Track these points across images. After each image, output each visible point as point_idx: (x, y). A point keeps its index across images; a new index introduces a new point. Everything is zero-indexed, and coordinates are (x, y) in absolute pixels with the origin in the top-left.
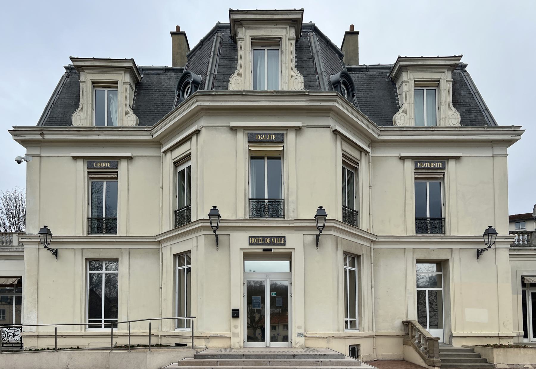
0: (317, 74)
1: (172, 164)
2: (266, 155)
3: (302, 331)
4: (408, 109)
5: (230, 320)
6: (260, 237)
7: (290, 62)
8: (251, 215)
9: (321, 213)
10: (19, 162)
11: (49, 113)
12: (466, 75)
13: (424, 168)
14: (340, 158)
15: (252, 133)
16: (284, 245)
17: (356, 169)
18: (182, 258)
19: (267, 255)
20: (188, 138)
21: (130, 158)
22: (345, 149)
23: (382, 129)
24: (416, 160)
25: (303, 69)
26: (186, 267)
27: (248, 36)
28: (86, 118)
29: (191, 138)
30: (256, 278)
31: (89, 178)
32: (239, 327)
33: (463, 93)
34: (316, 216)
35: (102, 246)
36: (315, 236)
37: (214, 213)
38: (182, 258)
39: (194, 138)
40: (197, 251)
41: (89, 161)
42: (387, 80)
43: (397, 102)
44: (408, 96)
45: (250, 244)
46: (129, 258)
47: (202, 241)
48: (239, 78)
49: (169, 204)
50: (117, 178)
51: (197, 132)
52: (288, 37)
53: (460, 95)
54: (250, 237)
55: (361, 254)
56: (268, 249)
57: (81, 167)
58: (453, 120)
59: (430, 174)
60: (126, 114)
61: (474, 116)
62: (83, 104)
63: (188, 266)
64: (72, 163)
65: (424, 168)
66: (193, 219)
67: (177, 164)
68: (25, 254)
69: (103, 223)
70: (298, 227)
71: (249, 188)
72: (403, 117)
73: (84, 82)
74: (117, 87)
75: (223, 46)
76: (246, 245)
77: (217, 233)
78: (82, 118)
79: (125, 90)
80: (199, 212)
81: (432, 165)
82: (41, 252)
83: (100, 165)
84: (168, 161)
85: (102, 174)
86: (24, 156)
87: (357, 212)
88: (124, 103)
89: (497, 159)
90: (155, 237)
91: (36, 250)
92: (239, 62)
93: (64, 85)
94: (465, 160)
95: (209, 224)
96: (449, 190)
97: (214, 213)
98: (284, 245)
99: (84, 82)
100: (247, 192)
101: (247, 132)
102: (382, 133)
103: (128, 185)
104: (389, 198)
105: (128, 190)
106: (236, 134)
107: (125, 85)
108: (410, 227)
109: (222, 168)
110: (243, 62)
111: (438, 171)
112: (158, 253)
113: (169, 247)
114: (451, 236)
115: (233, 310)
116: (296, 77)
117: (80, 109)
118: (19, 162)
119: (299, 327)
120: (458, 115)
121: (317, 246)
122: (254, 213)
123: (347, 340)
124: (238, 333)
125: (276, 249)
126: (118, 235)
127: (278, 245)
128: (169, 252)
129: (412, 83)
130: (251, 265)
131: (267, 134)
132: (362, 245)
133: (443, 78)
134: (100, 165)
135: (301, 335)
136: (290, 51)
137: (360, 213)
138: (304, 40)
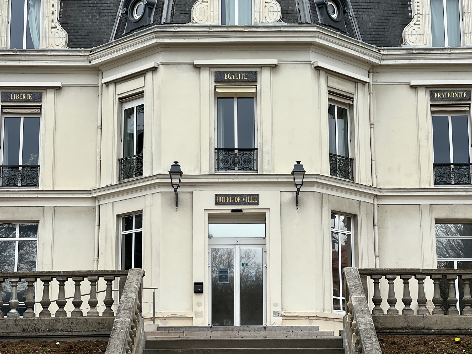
1: (117, 100)
2: (236, 99)
3: (278, 309)
5: (192, 296)
8: (218, 168)
9: (299, 169)
13: (442, 99)
14: (325, 96)
15: (219, 72)
16: (257, 204)
17: (351, 106)
18: (131, 220)
19: (237, 217)
20: (142, 74)
21: (58, 89)
22: (331, 84)
26: (134, 231)
29: (146, 73)
30: (223, 246)
32: (203, 305)
34: (293, 172)
36: (295, 194)
37: (176, 170)
38: (131, 220)
40: (151, 211)
43: (409, 9)
45: (216, 204)
46: (54, 220)
47: (158, 199)
49: (112, 149)
50: (40, 114)
51: (154, 70)
54: (216, 195)
55: (358, 213)
56: (238, 209)
60: (53, 30)
63: (138, 230)
65: (442, 99)
66: (146, 173)
67: (122, 100)
70: (274, 182)
71: (215, 136)
72: (414, 33)
76: (212, 205)
77: (178, 190)
80: (155, 163)
83: (18, 97)
84: (111, 96)
87: (352, 160)
88: (51, 15)
90: (90, 191)
95: (170, 181)
97: (176, 170)
98: (257, 204)
100: (213, 141)
102: (384, 57)
103: (55, 122)
105: (55, 129)
106: (200, 72)
108: (427, 178)
109: (182, 114)
111: (462, 103)
112: (94, 212)
113: (110, 206)
115: (196, 284)
119: (275, 305)
121: (297, 206)
122: (221, 165)
123: (335, 323)
124: (202, 312)
125: (247, 209)
127: (250, 204)
128: (110, 213)
130: (219, 229)
131: (238, 72)
132: (360, 201)
134: (18, 97)
135: (277, 314)
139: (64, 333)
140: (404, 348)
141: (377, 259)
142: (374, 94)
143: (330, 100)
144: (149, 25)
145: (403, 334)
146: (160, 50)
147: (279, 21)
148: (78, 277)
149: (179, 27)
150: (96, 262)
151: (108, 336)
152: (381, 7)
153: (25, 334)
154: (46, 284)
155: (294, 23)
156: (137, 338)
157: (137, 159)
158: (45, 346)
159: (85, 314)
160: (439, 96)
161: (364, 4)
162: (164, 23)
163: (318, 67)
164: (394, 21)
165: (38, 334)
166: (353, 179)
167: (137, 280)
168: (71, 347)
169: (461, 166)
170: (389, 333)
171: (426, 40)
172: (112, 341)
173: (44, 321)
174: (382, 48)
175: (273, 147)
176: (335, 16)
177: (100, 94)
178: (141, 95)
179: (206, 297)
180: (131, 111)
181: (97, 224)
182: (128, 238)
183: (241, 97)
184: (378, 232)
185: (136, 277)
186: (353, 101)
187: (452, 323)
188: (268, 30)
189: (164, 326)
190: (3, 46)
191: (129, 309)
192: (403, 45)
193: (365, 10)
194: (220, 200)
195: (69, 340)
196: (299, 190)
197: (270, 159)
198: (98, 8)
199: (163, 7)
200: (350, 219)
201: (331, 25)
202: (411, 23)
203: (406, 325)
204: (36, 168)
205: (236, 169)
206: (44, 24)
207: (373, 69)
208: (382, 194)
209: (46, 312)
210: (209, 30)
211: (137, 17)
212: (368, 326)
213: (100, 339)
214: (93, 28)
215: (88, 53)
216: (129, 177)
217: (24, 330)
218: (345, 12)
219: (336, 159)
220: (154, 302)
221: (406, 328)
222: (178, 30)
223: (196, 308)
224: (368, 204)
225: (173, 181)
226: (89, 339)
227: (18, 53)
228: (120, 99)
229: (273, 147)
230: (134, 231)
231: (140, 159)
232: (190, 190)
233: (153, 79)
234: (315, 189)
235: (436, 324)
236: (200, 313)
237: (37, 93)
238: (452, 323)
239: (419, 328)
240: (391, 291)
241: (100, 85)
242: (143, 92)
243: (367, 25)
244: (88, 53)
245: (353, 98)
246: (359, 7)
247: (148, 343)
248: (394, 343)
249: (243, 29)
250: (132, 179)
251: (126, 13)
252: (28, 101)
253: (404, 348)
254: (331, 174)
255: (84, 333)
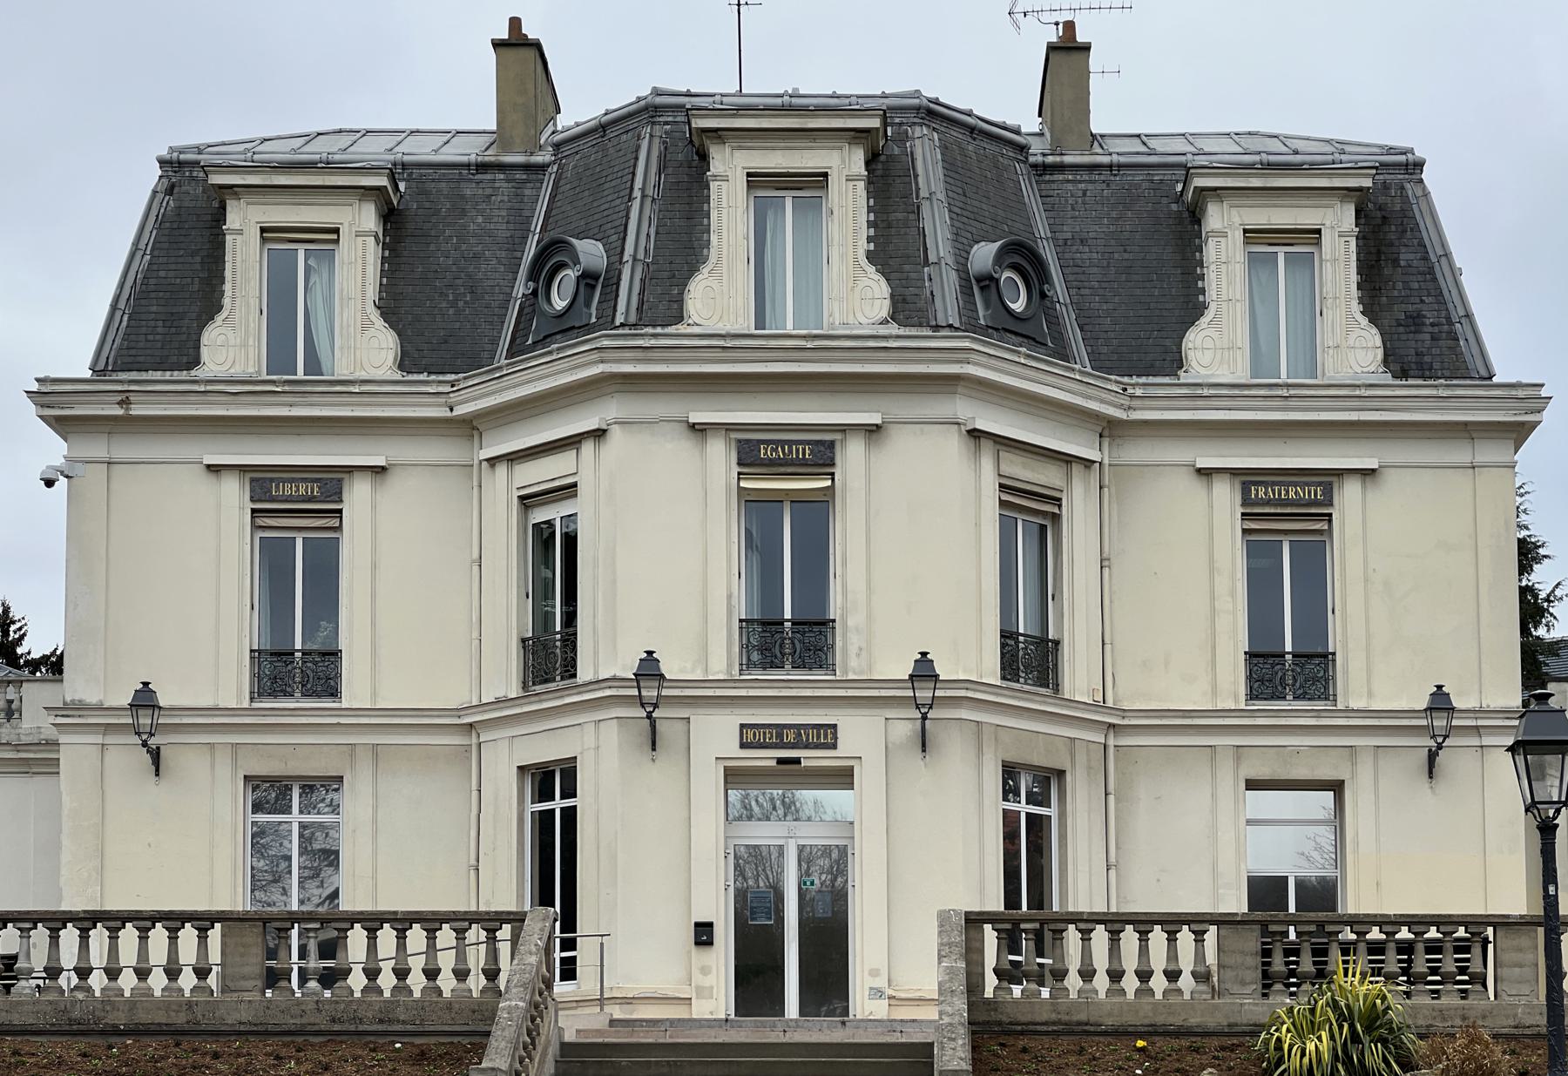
0: (926, 263)
1: (515, 500)
3: (881, 982)
4: (1225, 316)
5: (689, 952)
6: (770, 725)
7: (850, 241)
8: (749, 665)
9: (924, 671)
10: (49, 483)
11: (126, 318)
12: (1419, 193)
13: (1268, 503)
15: (748, 441)
16: (834, 746)
17: (1056, 518)
18: (550, 779)
20: (571, 443)
21: (379, 471)
22: (1006, 469)
23: (1139, 392)
24: (1246, 478)
25: (891, 247)
26: (558, 804)
27: (739, 169)
28: (245, 345)
31: (255, 527)
33: (1405, 257)
35: (297, 738)
37: (649, 669)
38: (550, 779)
39: (588, 448)
40: (597, 763)
41: (261, 481)
42: (1174, 207)
43: (1200, 284)
44: (1224, 277)
45: (743, 746)
48: (715, 285)
49: (507, 614)
50: (339, 528)
51: (599, 434)
52: (846, 172)
53: (1396, 262)
55: (1067, 766)
57: (234, 496)
58: (1360, 354)
59: (1288, 521)
60: (364, 329)
61: (1428, 337)
62: (233, 298)
63: (568, 803)
64: (206, 482)
65: (1268, 503)
66: (584, 673)
67: (528, 501)
68: (64, 756)
69: (297, 667)
71: (739, 590)
72: (1209, 343)
73: (240, 232)
74: (337, 241)
75: (670, 170)
76: (733, 749)
78: (232, 342)
79: (360, 253)
80: (604, 654)
81: (1292, 494)
82: (111, 755)
83: (288, 490)
84: (503, 488)
85: (297, 519)
86: (59, 461)
87: (1057, 643)
88: (359, 296)
89: (1485, 476)
90: (458, 712)
91: (95, 750)
92: (714, 238)
93: (161, 223)
94: (1391, 478)
95: (635, 692)
96: (1343, 569)
97: (649, 669)
98: (834, 746)
99: (240, 232)
100: (735, 601)
101: (734, 435)
102: (1135, 403)
104: (1162, 596)
105: (374, 566)
106: (704, 440)
107: (360, 239)
109: (666, 551)
110: (725, 240)
114: (1349, 712)
115: (697, 925)
116: (867, 282)
117: (224, 314)
118: (49, 483)
119: (874, 973)
120: (1373, 338)
122: (755, 656)
125: (811, 758)
126: (345, 704)
127: (818, 746)
128: (503, 761)
129: (1239, 235)
131: (790, 443)
133: (1328, 223)
134: (288, 490)
135: (877, 993)
136: (850, 209)
137: (1066, 648)
138: (897, 151)
139: (409, 1028)
140: (1039, 1060)
141: (1112, 873)
142: (1113, 490)
143: (1003, 504)
144: (587, 328)
145: (1047, 1033)
146: (614, 388)
147: (884, 322)
148: (432, 922)
149: (655, 336)
150: (472, 873)
151: (488, 1034)
152: (1135, 277)
153: (337, 1027)
154: (372, 934)
155: (921, 325)
156: (543, 1038)
157: (563, 640)
158: (374, 1050)
159: (447, 994)
160: (1261, 494)
161: (1095, 270)
162: (622, 325)
163: (975, 430)
164: (1165, 313)
165: (361, 1028)
166: (1057, 688)
167: (542, 930)
168: (423, 1053)
169: (1310, 656)
170: (1022, 1033)
171: (1235, 361)
172: (493, 1042)
173: (370, 1004)
174: (1135, 380)
175: (869, 617)
176: (1018, 306)
177: (475, 483)
178: (568, 491)
179: (722, 958)
180: (554, 558)
181: (474, 787)
182: (544, 821)
183: (799, 500)
184: (1116, 809)
185: (540, 925)
186: (1060, 506)
187: (1141, 1014)
188: (861, 346)
189: (628, 1017)
190: (251, 370)
191: (524, 985)
192: (1181, 373)
193: (1096, 285)
194: (751, 737)
195: (418, 1041)
196: (924, 717)
197: (864, 645)
198: (470, 277)
199: (619, 279)
200: (1048, 781)
201: (1009, 328)
202: (1203, 320)
203: (1054, 1016)
204: (332, 655)
205: (788, 667)
206: (345, 315)
207: (1110, 429)
208: (1126, 722)
209: (372, 988)
210: (726, 344)
211: (559, 304)
212: (957, 1018)
213: (477, 1040)
214: (458, 325)
215: (448, 389)
216: (546, 681)
217: (333, 1021)
218: (1043, 295)
219: (1017, 642)
220: (602, 966)
221: (1054, 1023)
222: (653, 342)
223: (698, 978)
224: (1092, 746)
225: (644, 693)
226: (455, 1040)
227: (287, 388)
228: (522, 498)
229: (869, 617)
230: (558, 804)
231: (570, 641)
232: (684, 713)
233: (597, 456)
234: (964, 714)
235: (1110, 1015)
236: (710, 990)
237: (331, 482)
238: (1141, 1014)
239: (1079, 1023)
240: (1087, 953)
241: (476, 462)
242: (575, 485)
243: (1100, 321)
244: (448, 389)
245: (1060, 500)
246: (1082, 277)
247: (566, 1048)
248: (1024, 1050)
249: (802, 343)
250: (552, 686)
251: (535, 293)
252: (311, 500)
253: (1039, 1060)
254: (1004, 678)
255: (446, 1028)
